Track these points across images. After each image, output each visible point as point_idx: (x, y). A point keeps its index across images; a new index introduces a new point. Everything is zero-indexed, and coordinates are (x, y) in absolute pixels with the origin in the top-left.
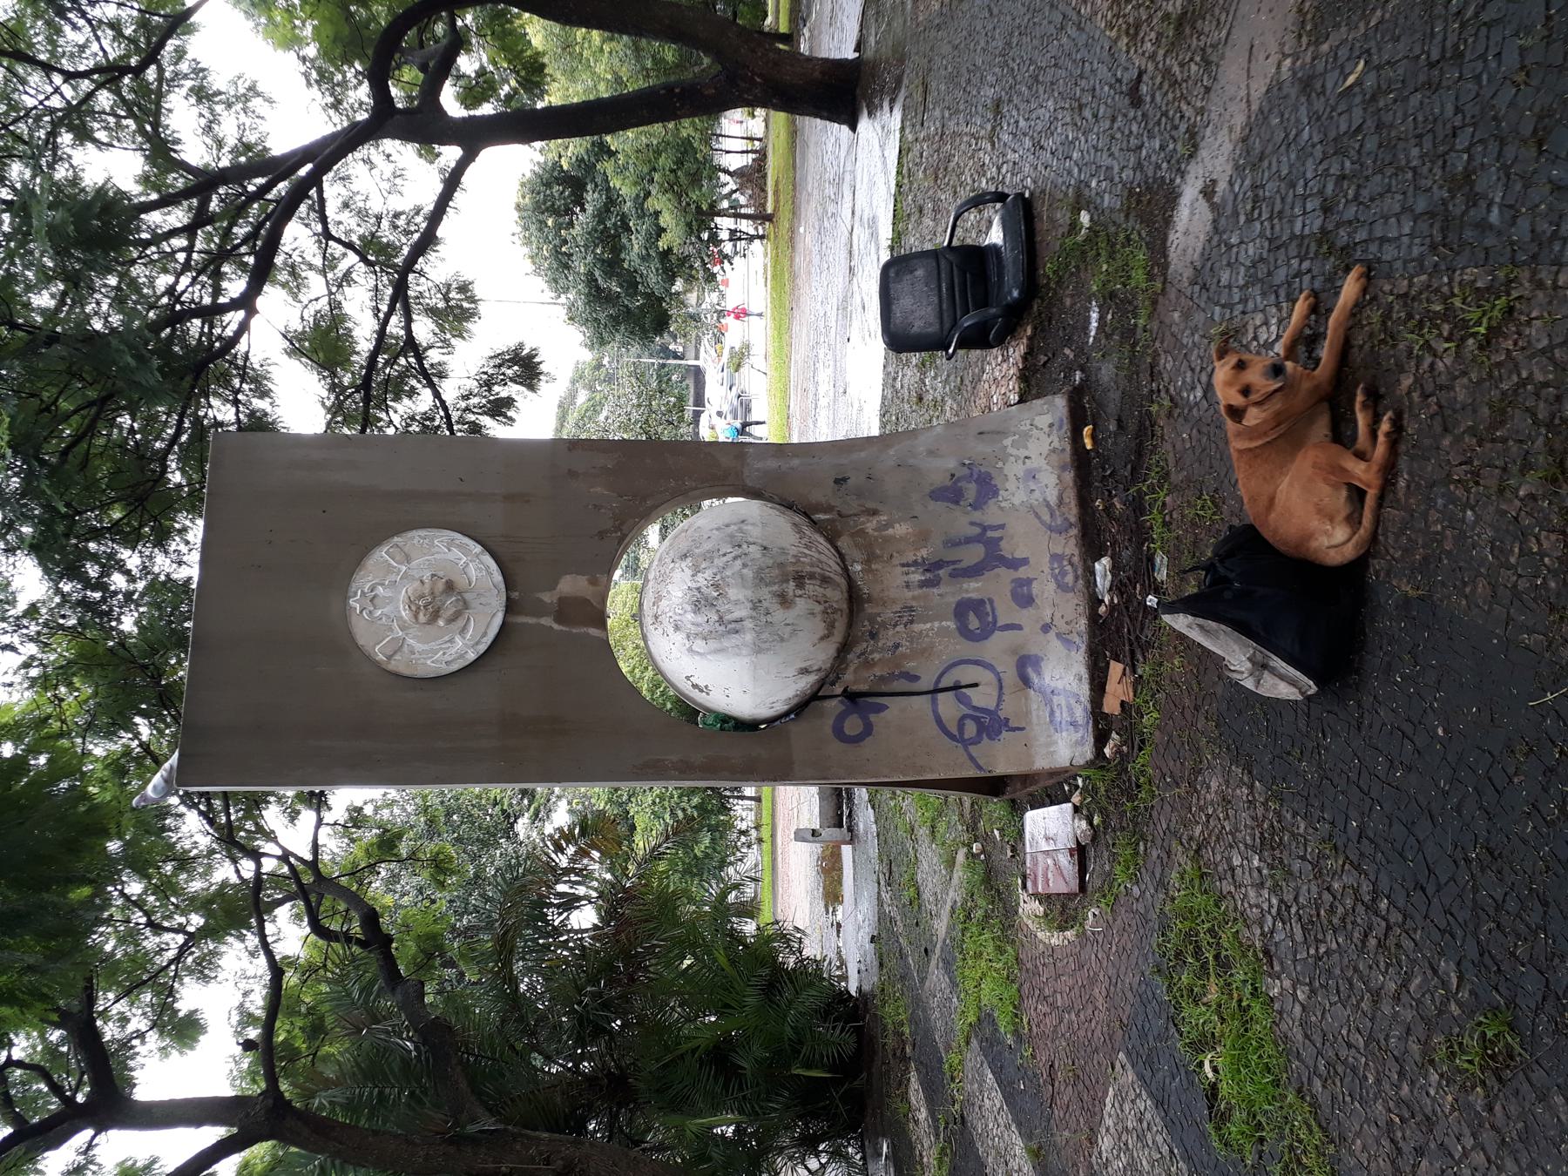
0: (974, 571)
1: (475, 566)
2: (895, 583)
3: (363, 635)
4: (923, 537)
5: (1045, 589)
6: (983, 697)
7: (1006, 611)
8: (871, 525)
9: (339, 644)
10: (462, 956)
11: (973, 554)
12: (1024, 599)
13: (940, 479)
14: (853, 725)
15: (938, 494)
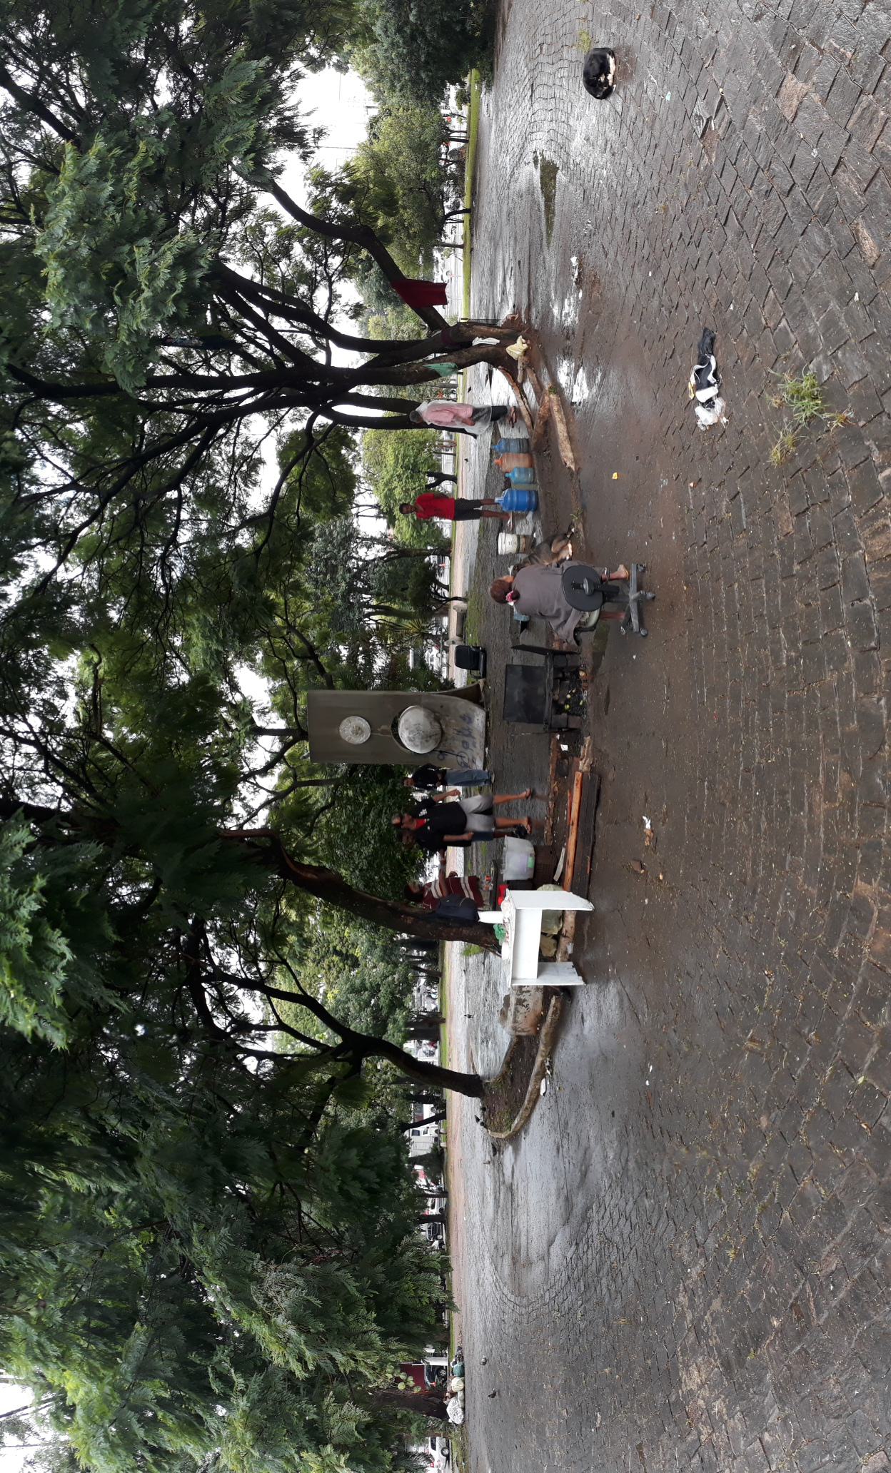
1: (364, 724)
2: (451, 732)
6: (466, 760)
9: (339, 737)
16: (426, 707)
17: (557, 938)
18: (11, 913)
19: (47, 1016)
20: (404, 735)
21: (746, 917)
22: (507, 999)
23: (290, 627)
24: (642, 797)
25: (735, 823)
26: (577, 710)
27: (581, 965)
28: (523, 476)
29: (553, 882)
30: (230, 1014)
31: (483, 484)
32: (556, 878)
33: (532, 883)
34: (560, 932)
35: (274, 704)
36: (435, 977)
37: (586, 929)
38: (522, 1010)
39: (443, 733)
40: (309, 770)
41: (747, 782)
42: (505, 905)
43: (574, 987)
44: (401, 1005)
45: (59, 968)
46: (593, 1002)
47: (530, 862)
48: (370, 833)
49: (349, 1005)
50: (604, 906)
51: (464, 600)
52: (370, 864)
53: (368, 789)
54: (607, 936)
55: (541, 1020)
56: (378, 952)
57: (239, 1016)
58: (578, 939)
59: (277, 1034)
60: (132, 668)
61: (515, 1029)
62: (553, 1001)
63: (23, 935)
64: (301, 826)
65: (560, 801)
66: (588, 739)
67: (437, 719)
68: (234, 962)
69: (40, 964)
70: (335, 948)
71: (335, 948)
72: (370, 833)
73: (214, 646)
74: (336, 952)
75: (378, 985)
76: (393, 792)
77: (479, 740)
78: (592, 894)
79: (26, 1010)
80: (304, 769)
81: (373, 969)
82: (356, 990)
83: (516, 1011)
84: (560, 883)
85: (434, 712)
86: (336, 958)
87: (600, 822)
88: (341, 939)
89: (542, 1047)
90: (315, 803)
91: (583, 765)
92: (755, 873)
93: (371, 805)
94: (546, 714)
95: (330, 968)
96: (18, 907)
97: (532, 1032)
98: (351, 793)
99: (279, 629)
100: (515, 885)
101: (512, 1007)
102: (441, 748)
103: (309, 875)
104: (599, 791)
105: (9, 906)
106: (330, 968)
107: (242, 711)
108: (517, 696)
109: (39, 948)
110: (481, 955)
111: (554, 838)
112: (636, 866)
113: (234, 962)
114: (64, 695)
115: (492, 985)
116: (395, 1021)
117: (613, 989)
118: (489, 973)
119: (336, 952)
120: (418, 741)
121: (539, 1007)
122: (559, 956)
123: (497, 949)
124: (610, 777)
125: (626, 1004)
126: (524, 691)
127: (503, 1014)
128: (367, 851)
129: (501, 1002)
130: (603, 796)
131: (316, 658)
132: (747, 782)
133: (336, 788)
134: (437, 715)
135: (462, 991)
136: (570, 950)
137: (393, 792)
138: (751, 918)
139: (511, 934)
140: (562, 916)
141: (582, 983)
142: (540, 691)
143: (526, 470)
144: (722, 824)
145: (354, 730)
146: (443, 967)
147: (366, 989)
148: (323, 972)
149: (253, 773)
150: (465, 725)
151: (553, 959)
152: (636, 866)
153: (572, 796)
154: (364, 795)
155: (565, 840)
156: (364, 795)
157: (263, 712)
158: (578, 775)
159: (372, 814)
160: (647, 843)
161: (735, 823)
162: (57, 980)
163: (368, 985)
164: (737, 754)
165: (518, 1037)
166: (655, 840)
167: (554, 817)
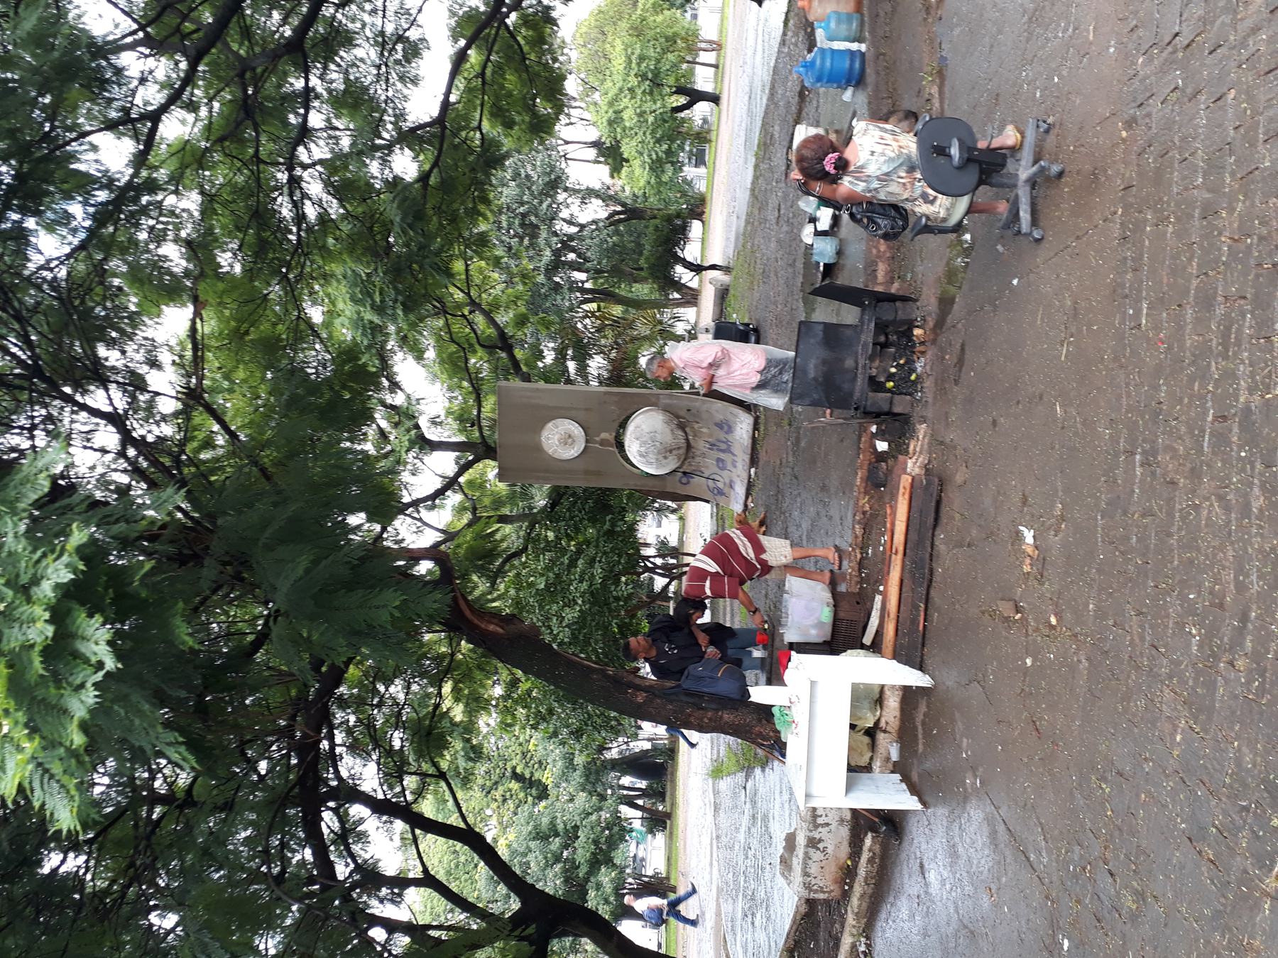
0: (723, 451)
1: (577, 431)
2: (701, 445)
3: (546, 448)
4: (711, 435)
5: (740, 465)
6: (720, 485)
7: (729, 466)
8: (696, 426)
9: (538, 448)
10: (537, 227)
11: (723, 446)
12: (734, 464)
13: (718, 421)
14: (684, 480)
15: (717, 424)
16: (667, 410)
17: (871, 733)
18: (25, 591)
19: (57, 768)
20: (633, 448)
21: (1231, 663)
22: (790, 840)
23: (475, 305)
24: (1016, 498)
25: (1197, 508)
26: (906, 385)
27: (915, 777)
28: (844, 27)
29: (863, 647)
30: (353, 856)
31: (767, 78)
32: (867, 640)
33: (834, 644)
34: (877, 723)
35: (449, 413)
36: (659, 821)
37: (919, 717)
38: (817, 856)
39: (689, 446)
40: (494, 502)
41: (1221, 439)
42: (788, 676)
43: (903, 814)
44: (609, 861)
45: (89, 685)
46: (939, 841)
47: (826, 615)
48: (578, 588)
49: (531, 857)
50: (951, 679)
51: (726, 269)
52: (574, 637)
53: (577, 530)
54: (960, 726)
55: (848, 873)
56: (577, 777)
57: (366, 861)
58: (906, 734)
59: (425, 892)
60: (257, 333)
61: (808, 887)
62: (868, 841)
63: (39, 625)
64: (482, 571)
65: (872, 523)
66: (922, 429)
67: (682, 427)
68: (369, 776)
69: (57, 679)
70: (514, 768)
71: (514, 768)
72: (578, 588)
73: (369, 315)
74: (516, 777)
75: (576, 828)
76: (610, 534)
77: (742, 458)
78: (928, 662)
79: (19, 749)
80: (487, 501)
81: (569, 802)
82: (542, 836)
83: (807, 857)
84: (875, 647)
85: (678, 417)
86: (514, 785)
87: (941, 547)
88: (524, 755)
89: (850, 919)
90: (502, 540)
91: (913, 466)
92: (1241, 587)
93: (579, 552)
94: (857, 395)
95: (505, 800)
96: (36, 581)
97: (836, 893)
98: (551, 535)
99: (459, 306)
100: (805, 648)
101: (800, 851)
102: (686, 468)
103: (491, 627)
104: (938, 503)
105: (24, 579)
106: (505, 800)
107: (404, 416)
108: (813, 369)
109: (62, 650)
110: (740, 777)
111: (862, 581)
112: (1006, 608)
113: (369, 776)
114: (154, 364)
115: (760, 819)
116: (599, 886)
117: (976, 814)
118: (754, 803)
119: (516, 777)
120: (652, 458)
121: (845, 850)
122: (877, 765)
123: (778, 748)
124: (959, 478)
125: (1001, 828)
126: (824, 362)
127: (785, 862)
128: (570, 615)
129: (779, 847)
130: (944, 510)
131: (508, 348)
132: (1221, 439)
133: (532, 527)
134: (682, 421)
135: (706, 840)
136: (895, 756)
137: (610, 534)
138: (1240, 663)
139: (803, 728)
140: (878, 698)
141: (919, 807)
142: (849, 363)
143: (849, 18)
144: (1170, 514)
145: (562, 440)
146: (673, 804)
147: (557, 835)
148: (494, 805)
149: (415, 504)
150: (722, 436)
151: (868, 769)
152: (1006, 608)
153: (894, 513)
154: (570, 538)
155: (882, 578)
156: (570, 538)
157: (434, 422)
158: (905, 481)
159: (580, 562)
160: (1027, 569)
161: (1197, 508)
162: (82, 703)
163: (560, 827)
164: (1202, 398)
165: (809, 902)
166: (1042, 561)
167: (863, 549)
